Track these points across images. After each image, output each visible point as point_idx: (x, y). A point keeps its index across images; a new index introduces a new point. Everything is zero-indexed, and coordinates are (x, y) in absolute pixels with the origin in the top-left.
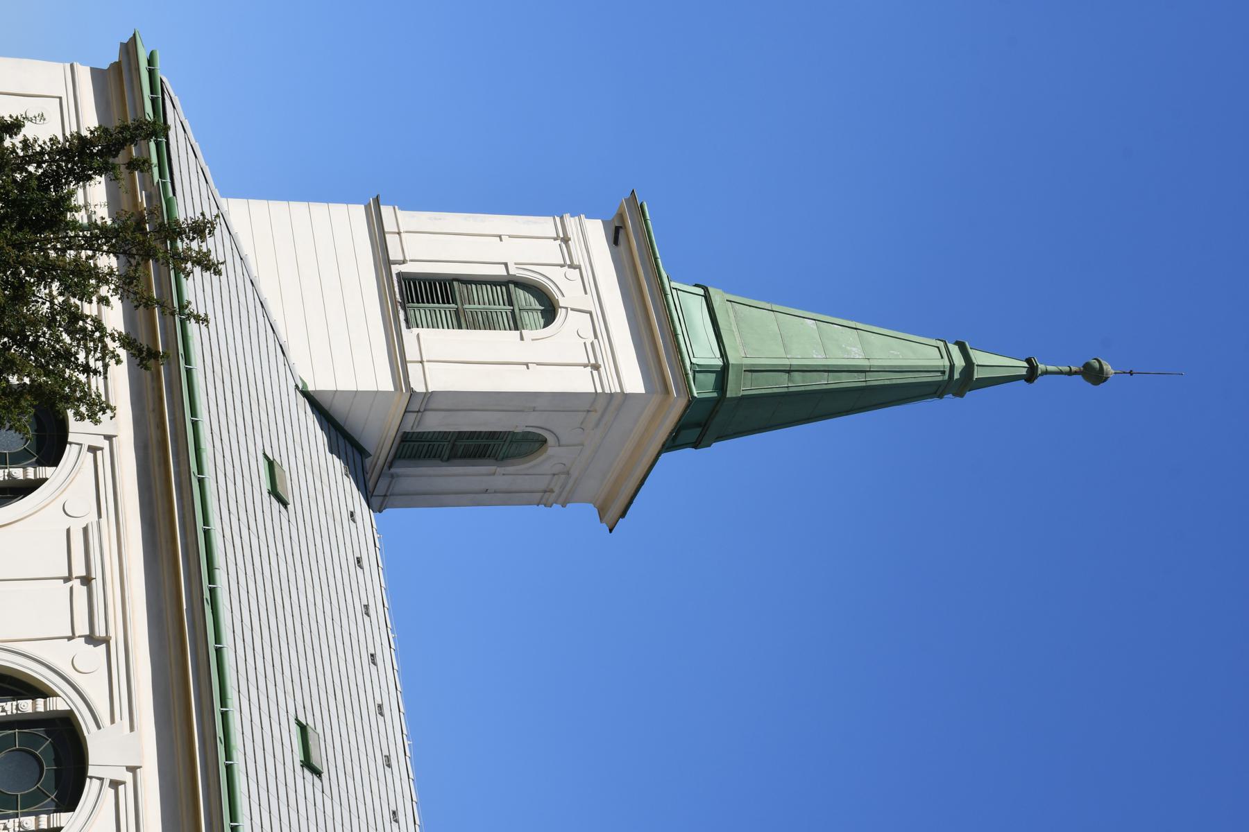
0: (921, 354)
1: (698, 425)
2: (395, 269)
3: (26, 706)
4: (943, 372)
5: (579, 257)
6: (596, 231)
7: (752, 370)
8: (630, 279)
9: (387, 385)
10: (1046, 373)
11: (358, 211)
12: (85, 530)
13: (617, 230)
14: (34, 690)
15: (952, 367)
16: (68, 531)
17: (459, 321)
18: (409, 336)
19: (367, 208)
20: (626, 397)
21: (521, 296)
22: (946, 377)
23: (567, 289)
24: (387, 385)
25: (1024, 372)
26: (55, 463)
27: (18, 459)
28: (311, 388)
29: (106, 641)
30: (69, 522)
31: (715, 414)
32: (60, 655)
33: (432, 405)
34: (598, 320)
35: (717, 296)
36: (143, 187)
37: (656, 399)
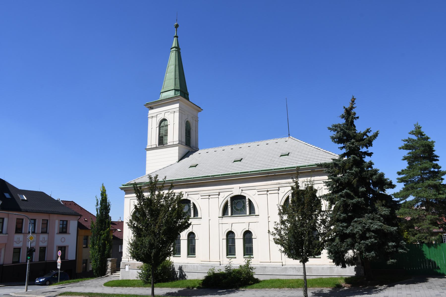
0: (173, 56)
2: (157, 146)
3: (229, 204)
6: (151, 112)
17: (166, 135)
18: (169, 144)
20: (180, 107)
21: (162, 125)
23: (161, 117)
27: (190, 206)
29: (219, 193)
30: (200, 199)
31: (183, 91)
34: (166, 112)
35: (162, 91)
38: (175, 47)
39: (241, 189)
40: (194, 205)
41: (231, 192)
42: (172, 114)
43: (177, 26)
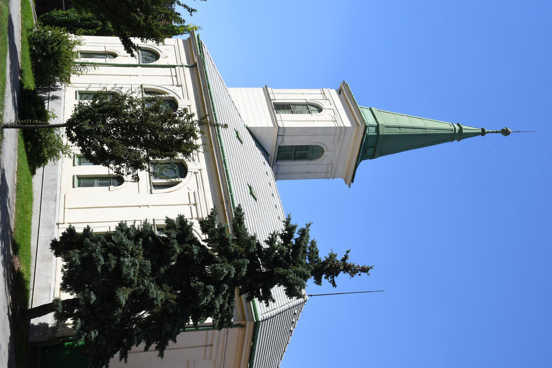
0: (444, 126)
1: (372, 147)
2: (272, 102)
4: (452, 130)
5: (328, 96)
7: (387, 127)
8: (345, 102)
9: (271, 125)
10: (488, 132)
11: (261, 90)
12: (194, 193)
13: (340, 91)
14: (164, 93)
15: (455, 129)
16: (189, 193)
18: (278, 116)
19: (263, 89)
20: (346, 128)
21: (311, 108)
22: (453, 132)
23: (325, 104)
24: (271, 125)
25: (480, 131)
26: (185, 177)
27: (175, 177)
28: (249, 126)
29: (181, 86)
30: (189, 191)
31: (375, 144)
32: (171, 88)
33: (286, 133)
34: (335, 111)
35: (374, 109)
36: (196, 56)
37: (355, 128)
38: (461, 129)
39: (199, 172)
40: (177, 183)
41: (182, 97)
42: (333, 115)
43: (505, 132)
